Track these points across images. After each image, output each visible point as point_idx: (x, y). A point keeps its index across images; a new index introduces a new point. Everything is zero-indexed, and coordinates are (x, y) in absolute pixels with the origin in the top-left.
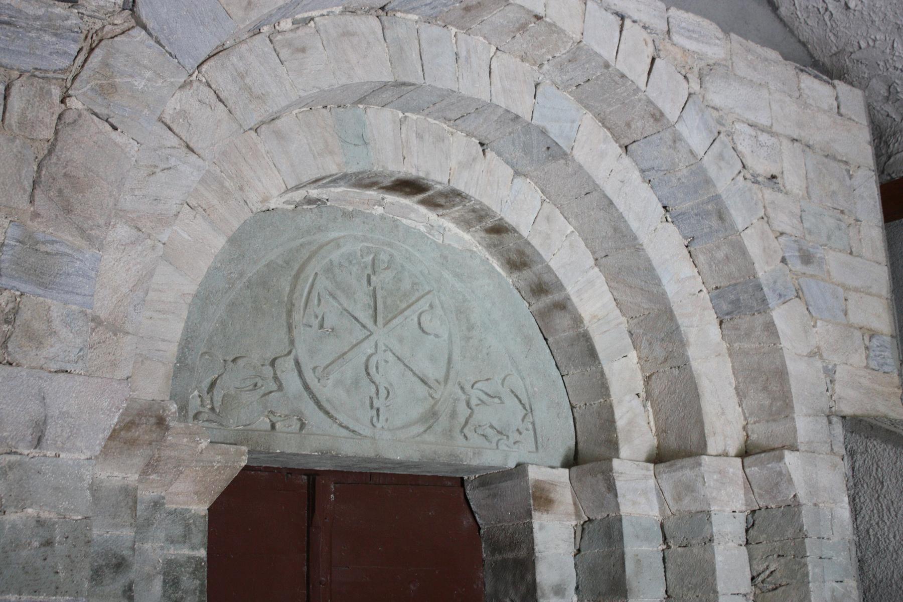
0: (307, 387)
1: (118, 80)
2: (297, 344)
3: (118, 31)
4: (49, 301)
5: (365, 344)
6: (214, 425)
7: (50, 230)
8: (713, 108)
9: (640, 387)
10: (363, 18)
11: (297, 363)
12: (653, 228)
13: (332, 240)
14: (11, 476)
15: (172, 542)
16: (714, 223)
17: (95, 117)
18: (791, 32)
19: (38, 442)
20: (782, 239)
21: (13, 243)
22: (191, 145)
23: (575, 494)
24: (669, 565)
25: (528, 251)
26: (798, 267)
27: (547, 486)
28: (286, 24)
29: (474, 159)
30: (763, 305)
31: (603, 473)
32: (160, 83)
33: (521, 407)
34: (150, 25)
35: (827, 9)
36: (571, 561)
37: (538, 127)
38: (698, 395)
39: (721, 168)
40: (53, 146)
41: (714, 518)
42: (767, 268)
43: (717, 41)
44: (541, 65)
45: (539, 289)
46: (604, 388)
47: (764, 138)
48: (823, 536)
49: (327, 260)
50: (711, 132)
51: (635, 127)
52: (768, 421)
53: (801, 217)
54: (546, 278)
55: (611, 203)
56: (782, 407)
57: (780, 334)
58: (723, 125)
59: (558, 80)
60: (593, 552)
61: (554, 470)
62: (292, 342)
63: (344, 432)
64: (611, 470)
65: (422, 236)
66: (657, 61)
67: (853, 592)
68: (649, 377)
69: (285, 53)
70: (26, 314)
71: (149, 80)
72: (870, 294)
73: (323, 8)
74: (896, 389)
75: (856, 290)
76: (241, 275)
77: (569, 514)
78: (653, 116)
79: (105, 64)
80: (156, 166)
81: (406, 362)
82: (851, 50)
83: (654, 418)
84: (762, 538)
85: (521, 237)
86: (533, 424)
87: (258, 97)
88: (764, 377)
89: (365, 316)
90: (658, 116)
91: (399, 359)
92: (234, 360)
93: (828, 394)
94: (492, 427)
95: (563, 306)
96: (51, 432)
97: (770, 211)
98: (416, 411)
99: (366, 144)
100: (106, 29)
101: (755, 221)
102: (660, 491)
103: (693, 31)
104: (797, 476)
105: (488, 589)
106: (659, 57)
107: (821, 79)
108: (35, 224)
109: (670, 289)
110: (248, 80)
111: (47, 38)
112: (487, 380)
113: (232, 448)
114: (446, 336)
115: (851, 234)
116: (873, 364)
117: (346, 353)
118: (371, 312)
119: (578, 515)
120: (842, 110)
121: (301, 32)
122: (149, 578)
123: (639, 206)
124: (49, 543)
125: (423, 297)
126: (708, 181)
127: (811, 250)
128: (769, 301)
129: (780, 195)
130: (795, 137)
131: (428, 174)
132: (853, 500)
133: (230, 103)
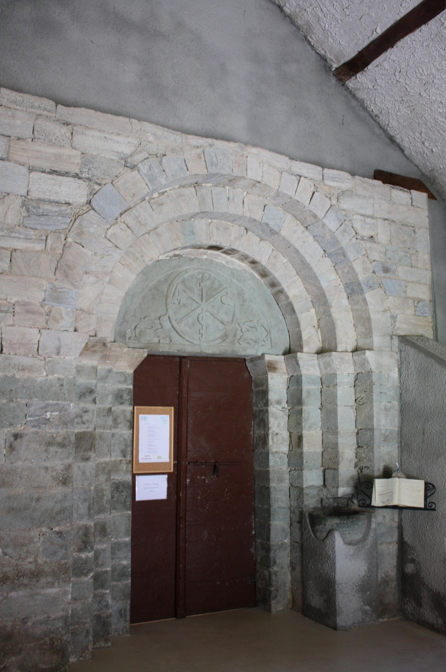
0: (173, 327)
1: (84, 230)
2: (169, 311)
3: (85, 212)
4: (61, 308)
5: (197, 310)
6: (136, 342)
7: (61, 284)
8: (343, 210)
9: (315, 323)
10: (188, 188)
11: (169, 318)
12: (317, 260)
13: (184, 270)
14: (49, 364)
15: (120, 383)
16: (342, 258)
17: (76, 244)
18: (411, 161)
19: (58, 354)
20: (374, 263)
21: (49, 289)
22: (117, 245)
23: (287, 365)
24: (322, 394)
25: (266, 270)
26: (382, 274)
28: (156, 195)
29: (242, 236)
30: (362, 291)
31: (294, 358)
32: (99, 229)
33: (265, 331)
34: (96, 209)
35: (424, 152)
36: (285, 392)
37: (264, 223)
38: (335, 328)
39: (344, 236)
40: (62, 255)
41: (338, 376)
42: (364, 276)
43: (348, 181)
44: (266, 198)
45: (273, 285)
46: (298, 324)
47: (368, 220)
48: (382, 384)
49: (182, 278)
50: (340, 221)
51: (308, 221)
52: (364, 338)
53: (385, 253)
54: (274, 281)
55: (298, 251)
56: (368, 333)
57: (368, 303)
58: (347, 217)
59: (274, 203)
60: (293, 388)
61: (277, 357)
62: (167, 310)
63: (188, 343)
64: (296, 357)
65: (224, 266)
66: (315, 193)
67: (396, 406)
69: (154, 207)
70: (53, 313)
71: (95, 228)
72: (420, 283)
73: (170, 187)
74: (430, 324)
75: (412, 282)
76: (147, 286)
77: (284, 373)
78: (313, 216)
79: (80, 225)
80: (104, 255)
81: (215, 315)
82: (437, 169)
83: (321, 335)
84: (360, 384)
85: (262, 265)
86: (271, 338)
87: (144, 225)
89: (197, 299)
90: (315, 216)
91: (212, 314)
92: (144, 318)
93: (392, 327)
94: (251, 339)
95: (281, 291)
96: (62, 350)
97: (369, 252)
98: (219, 334)
99: (194, 234)
100: (80, 212)
101: (360, 257)
102: (319, 365)
103: (336, 178)
104: (370, 360)
105: (254, 401)
106: (317, 191)
107: (404, 191)
108: (56, 282)
109: (324, 285)
110: (140, 219)
111: (59, 218)
112: (251, 321)
113: (141, 350)
114: (233, 305)
115: (412, 258)
116: (418, 313)
117: (189, 313)
118: (201, 297)
120: (414, 204)
121: (161, 197)
122: (107, 395)
123: (311, 251)
124: (62, 385)
125: (222, 290)
126: (338, 242)
127: (389, 267)
128: (364, 290)
129: (375, 244)
130: (386, 218)
131: (221, 243)
132: (400, 370)
133: (132, 228)
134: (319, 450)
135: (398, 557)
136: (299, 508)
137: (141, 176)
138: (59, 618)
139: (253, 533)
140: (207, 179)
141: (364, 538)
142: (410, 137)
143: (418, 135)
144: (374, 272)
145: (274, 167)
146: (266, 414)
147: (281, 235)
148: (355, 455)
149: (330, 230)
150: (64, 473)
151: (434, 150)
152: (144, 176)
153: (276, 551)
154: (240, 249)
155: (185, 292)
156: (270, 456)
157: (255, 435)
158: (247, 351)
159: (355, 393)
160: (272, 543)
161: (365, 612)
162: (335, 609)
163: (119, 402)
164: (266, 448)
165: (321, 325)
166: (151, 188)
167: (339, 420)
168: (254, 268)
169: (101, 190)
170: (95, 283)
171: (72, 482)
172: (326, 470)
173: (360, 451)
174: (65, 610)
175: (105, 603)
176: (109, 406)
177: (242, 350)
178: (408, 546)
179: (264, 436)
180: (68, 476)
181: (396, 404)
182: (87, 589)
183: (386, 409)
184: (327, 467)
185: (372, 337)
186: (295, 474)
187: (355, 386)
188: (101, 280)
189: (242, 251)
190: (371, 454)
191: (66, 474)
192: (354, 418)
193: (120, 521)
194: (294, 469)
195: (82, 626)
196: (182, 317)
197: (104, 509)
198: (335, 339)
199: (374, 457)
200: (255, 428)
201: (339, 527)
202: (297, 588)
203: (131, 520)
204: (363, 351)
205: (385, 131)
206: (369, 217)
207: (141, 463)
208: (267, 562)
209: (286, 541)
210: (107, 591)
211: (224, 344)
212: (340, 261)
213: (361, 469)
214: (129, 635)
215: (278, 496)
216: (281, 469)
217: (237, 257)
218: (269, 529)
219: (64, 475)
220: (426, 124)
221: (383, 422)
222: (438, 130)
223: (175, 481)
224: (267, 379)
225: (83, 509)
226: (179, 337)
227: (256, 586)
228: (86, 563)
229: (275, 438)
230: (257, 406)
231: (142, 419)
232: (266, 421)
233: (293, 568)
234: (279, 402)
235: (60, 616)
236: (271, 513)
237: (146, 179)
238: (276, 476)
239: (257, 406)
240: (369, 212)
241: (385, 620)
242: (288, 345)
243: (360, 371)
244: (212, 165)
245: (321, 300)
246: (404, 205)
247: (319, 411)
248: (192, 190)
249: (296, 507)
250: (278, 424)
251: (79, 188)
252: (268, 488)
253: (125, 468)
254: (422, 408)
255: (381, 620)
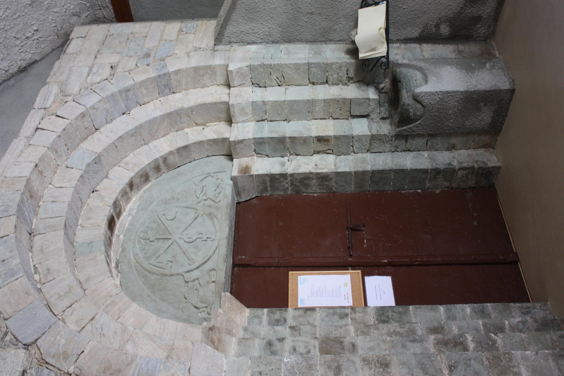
0: (197, 268)
1: (61, 351)
3: (38, 351)
5: (179, 243)
6: (213, 306)
10: (35, 243)
11: (187, 272)
15: (261, 323)
16: (131, 93)
18: (47, 55)
20: (139, 65)
22: (91, 318)
23: (244, 156)
24: (273, 119)
25: (141, 173)
26: (150, 60)
27: (240, 168)
28: (37, 277)
29: (100, 195)
30: (167, 75)
34: (36, 337)
35: (37, 39)
37: (86, 167)
39: (107, 90)
41: (255, 100)
44: (58, 165)
46: (200, 143)
47: (94, 70)
51: (88, 125)
54: (152, 166)
55: (121, 137)
56: (210, 70)
59: (65, 158)
60: (268, 150)
62: (178, 274)
68: (196, 124)
69: (50, 278)
71: (61, 338)
72: (164, 30)
73: (29, 260)
75: (162, 36)
76: (149, 296)
78: (83, 117)
84: (263, 81)
85: (134, 176)
86: (214, 173)
87: (70, 289)
88: (197, 76)
89: (168, 243)
90: (83, 115)
92: (186, 299)
94: (215, 190)
98: (208, 222)
99: (92, 242)
101: (131, 76)
102: (243, 121)
103: (45, 98)
104: (239, 65)
105: (282, 193)
107: (69, 44)
109: (159, 113)
110: (62, 294)
113: (223, 299)
114: (177, 209)
116: (193, 31)
117: (183, 252)
118: (166, 241)
119: (253, 156)
120: (83, 36)
121: (40, 270)
122: (275, 332)
126: (112, 95)
131: (106, 215)
132: (249, 44)
133: (73, 302)
134: (331, 122)
135: (435, 43)
136: (392, 140)
137: (4, 286)
138: (558, 364)
139: (419, 191)
140: (25, 220)
141: (420, 69)
142: (21, 51)
143: (18, 42)
144: (148, 65)
145: (22, 151)
146: (295, 176)
147: (101, 152)
148: (335, 86)
149: (99, 101)
150: (373, 366)
151: (36, 28)
152: (6, 282)
153: (437, 164)
154: (114, 197)
155: (159, 256)
156: (339, 171)
157: (318, 191)
158: (226, 196)
159: (272, 86)
160: (430, 167)
161: (493, 67)
162: (494, 91)
163: (283, 323)
164: (331, 177)
165: (202, 121)
166: (22, 275)
167: (300, 99)
168: (138, 187)
169: (14, 332)
170: (134, 343)
171: (384, 355)
172: (352, 114)
173: (331, 80)
174: (546, 358)
175: (521, 325)
176: (288, 329)
177: (227, 199)
178: (423, 31)
179: (319, 178)
180: (378, 361)
181: (282, 47)
182: (511, 340)
183: (288, 54)
184: (348, 113)
185: (215, 65)
186: (357, 146)
187: (265, 87)
188: (131, 336)
189: (117, 194)
190: (334, 67)
191: (375, 363)
192: (298, 87)
193: (421, 316)
194: (351, 148)
195: (557, 344)
196: (187, 259)
197: (412, 330)
198: (216, 104)
199: (337, 63)
200: (311, 191)
201: (410, 90)
202: (473, 141)
203: (420, 306)
204: (229, 73)
205: (13, 76)
206: (91, 70)
207: (353, 304)
208: (448, 173)
209: (426, 155)
210: (507, 323)
211: (219, 217)
212: (134, 97)
213: (350, 79)
214: (549, 303)
215: (381, 163)
216: (352, 161)
217: (124, 203)
218: (416, 170)
219: (376, 366)
220: (6, 30)
221: (302, 56)
222: (14, 19)
223: (370, 268)
224: (258, 176)
225: (415, 348)
226: (209, 262)
227: (473, 188)
228: (480, 342)
229: (320, 166)
230: (287, 188)
231: (304, 304)
232: (303, 176)
233: (453, 148)
234: (283, 164)
235: (555, 364)
236: (399, 168)
237: (9, 281)
238: (360, 165)
239: (287, 188)
240: (86, 70)
241: (496, 52)
242: (223, 157)
243: (250, 80)
244: (7, 211)
245: (175, 119)
246: (83, 44)
247: (291, 122)
248: (36, 239)
249: (391, 144)
250: (305, 164)
251: (4, 359)
252: (374, 172)
253: (361, 315)
254: (287, 16)
255: (498, 56)
